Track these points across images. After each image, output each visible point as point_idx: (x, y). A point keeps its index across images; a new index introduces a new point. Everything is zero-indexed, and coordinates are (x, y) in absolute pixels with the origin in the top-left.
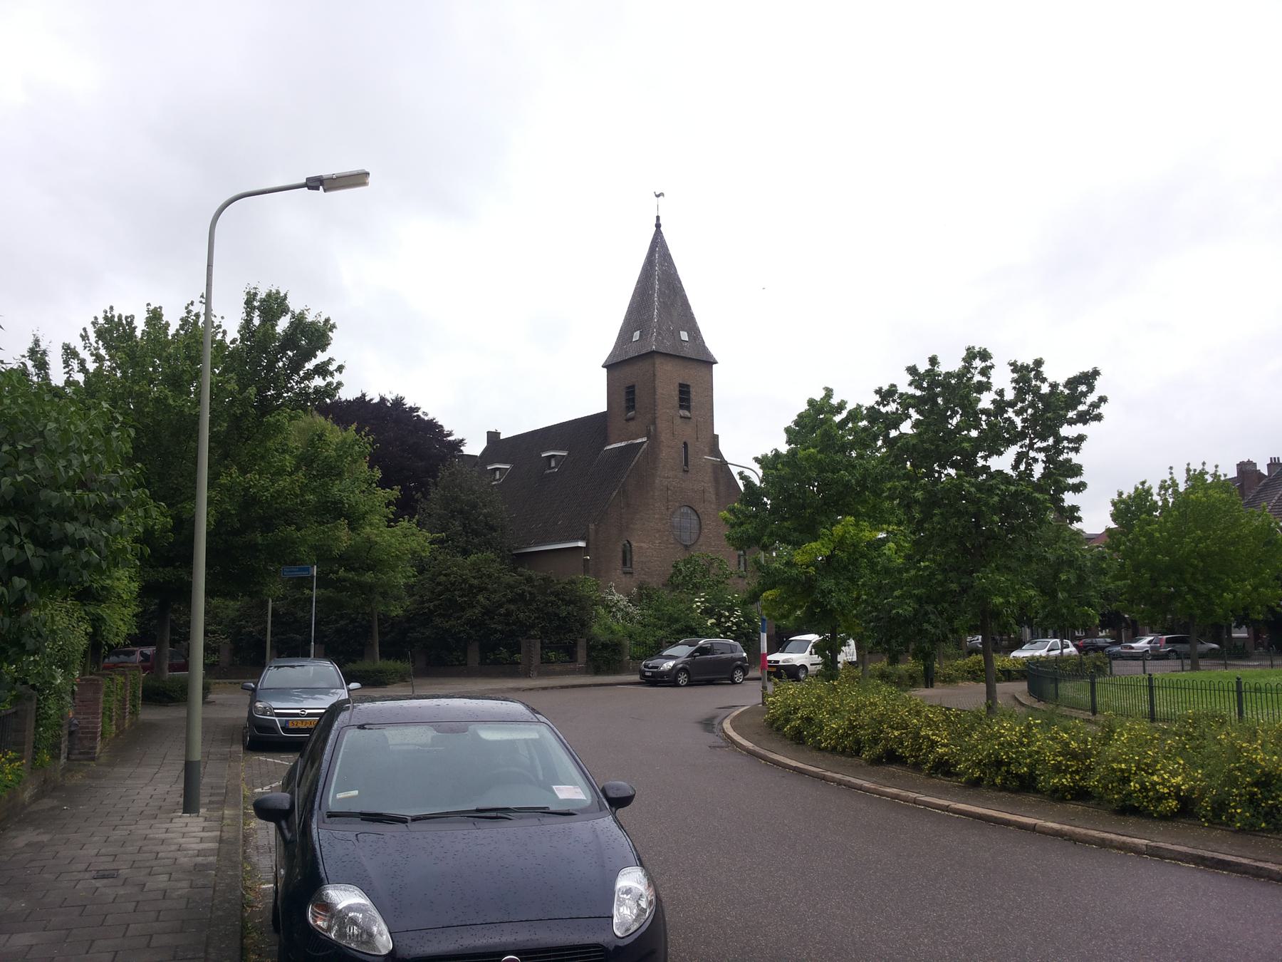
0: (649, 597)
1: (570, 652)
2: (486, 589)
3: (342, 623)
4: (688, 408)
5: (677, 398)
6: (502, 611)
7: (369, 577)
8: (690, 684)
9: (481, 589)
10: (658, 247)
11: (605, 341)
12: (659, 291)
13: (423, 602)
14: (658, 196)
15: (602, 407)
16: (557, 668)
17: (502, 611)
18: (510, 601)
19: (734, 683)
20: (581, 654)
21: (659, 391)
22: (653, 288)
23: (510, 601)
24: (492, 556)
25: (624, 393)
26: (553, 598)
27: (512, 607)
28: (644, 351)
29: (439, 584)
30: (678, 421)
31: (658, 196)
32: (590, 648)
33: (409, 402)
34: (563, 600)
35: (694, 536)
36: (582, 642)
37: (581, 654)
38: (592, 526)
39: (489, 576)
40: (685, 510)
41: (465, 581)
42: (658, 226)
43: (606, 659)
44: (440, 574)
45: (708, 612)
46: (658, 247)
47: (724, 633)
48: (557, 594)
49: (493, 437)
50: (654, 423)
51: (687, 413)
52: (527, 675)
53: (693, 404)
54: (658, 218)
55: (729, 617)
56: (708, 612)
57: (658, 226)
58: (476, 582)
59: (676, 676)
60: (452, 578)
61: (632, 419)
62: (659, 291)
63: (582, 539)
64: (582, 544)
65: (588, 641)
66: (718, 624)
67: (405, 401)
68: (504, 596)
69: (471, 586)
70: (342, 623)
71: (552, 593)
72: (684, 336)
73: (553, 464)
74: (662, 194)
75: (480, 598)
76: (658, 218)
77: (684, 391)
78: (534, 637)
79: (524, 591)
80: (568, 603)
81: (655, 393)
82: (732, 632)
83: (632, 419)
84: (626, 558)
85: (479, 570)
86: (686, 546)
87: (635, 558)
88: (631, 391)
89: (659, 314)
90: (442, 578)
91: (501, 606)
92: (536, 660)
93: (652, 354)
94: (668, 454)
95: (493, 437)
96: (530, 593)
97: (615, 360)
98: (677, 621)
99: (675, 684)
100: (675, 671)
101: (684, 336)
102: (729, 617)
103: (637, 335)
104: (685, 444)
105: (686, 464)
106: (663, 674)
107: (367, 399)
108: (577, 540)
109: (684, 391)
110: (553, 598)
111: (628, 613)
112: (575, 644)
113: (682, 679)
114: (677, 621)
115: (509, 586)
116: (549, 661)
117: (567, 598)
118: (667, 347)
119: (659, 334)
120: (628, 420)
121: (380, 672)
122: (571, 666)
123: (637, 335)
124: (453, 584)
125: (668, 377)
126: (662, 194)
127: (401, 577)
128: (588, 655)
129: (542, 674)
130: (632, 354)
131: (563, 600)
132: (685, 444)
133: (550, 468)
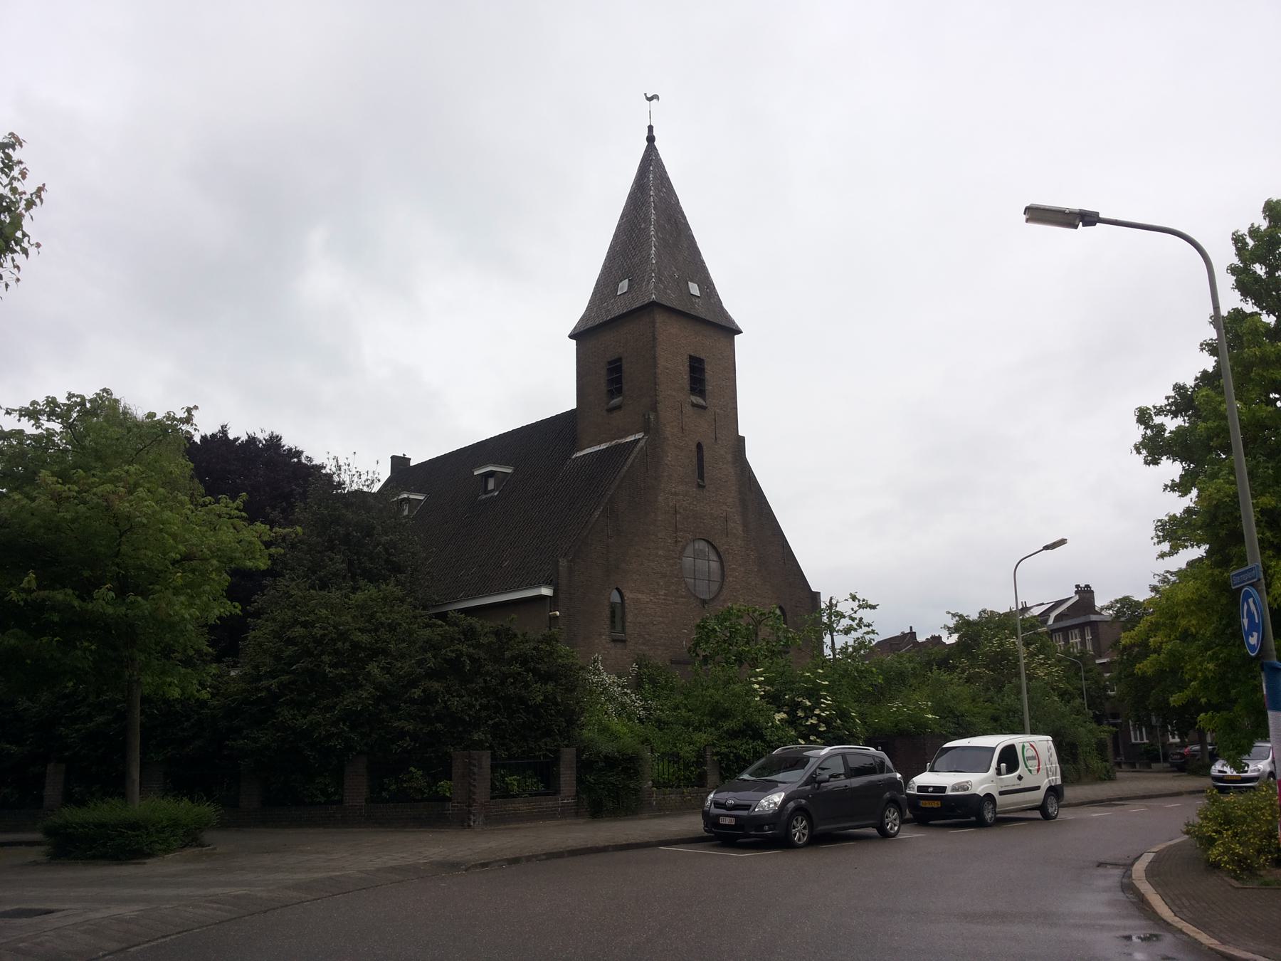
0: (653, 681)
1: (547, 776)
2: (385, 652)
3: (100, 719)
4: (702, 393)
5: (686, 377)
6: (417, 693)
7: (104, 601)
8: (817, 840)
9: (374, 653)
10: (651, 163)
11: (574, 302)
12: (653, 225)
13: (259, 679)
14: (650, 99)
15: (570, 403)
16: (521, 806)
17: (417, 693)
18: (432, 674)
19: (884, 834)
20: (567, 778)
21: (661, 363)
22: (646, 220)
23: (432, 674)
24: (398, 591)
25: (604, 372)
26: (516, 668)
27: (436, 685)
28: (638, 305)
29: (290, 641)
30: (688, 409)
31: (650, 99)
32: (584, 766)
33: (288, 442)
34: (535, 672)
35: (715, 587)
36: (568, 755)
37: (567, 778)
38: (563, 563)
39: (392, 628)
40: (702, 545)
41: (343, 636)
42: (651, 139)
43: (610, 787)
44: (295, 622)
45: (775, 700)
46: (651, 163)
47: (806, 738)
48: (524, 660)
49: (399, 463)
50: (654, 408)
51: (701, 401)
52: (462, 822)
53: (709, 388)
54: (650, 128)
55: (811, 709)
56: (775, 700)
57: (651, 139)
58: (365, 638)
59: (789, 827)
60: (318, 632)
61: (618, 408)
62: (653, 225)
63: (547, 583)
64: (546, 591)
65: (580, 752)
66: (792, 721)
67: (283, 442)
68: (420, 663)
69: (356, 646)
70: (100, 719)
71: (514, 658)
72: (694, 289)
73: (491, 485)
74: (655, 97)
75: (373, 668)
76: (650, 128)
77: (696, 368)
78: (479, 745)
79: (460, 654)
80: (545, 678)
81: (655, 366)
82: (819, 734)
83: (618, 408)
84: (617, 615)
85: (372, 616)
86: (704, 602)
87: (629, 618)
88: (615, 370)
89: (658, 255)
90: (299, 630)
91: (414, 683)
92: (482, 791)
93: (653, 305)
94: (676, 460)
95: (399, 463)
96: (470, 657)
97: (590, 324)
98: (726, 715)
99: (783, 842)
100: (780, 817)
101: (694, 289)
102: (811, 709)
103: (624, 286)
104: (699, 446)
105: (701, 476)
106: (760, 821)
107: (231, 437)
108: (538, 584)
109: (696, 368)
110: (516, 668)
111: (623, 705)
112: (557, 760)
113: (799, 831)
114: (726, 715)
115: (430, 646)
116: (506, 794)
117: (543, 668)
118: (671, 300)
119: (659, 280)
120: (610, 410)
121: (134, 826)
122: (547, 803)
123: (624, 286)
124: (318, 641)
125: (675, 347)
126: (655, 97)
127: (192, 609)
128: (580, 781)
129: (497, 820)
130: (617, 312)
131: (535, 672)
132: (699, 446)
133: (486, 491)
